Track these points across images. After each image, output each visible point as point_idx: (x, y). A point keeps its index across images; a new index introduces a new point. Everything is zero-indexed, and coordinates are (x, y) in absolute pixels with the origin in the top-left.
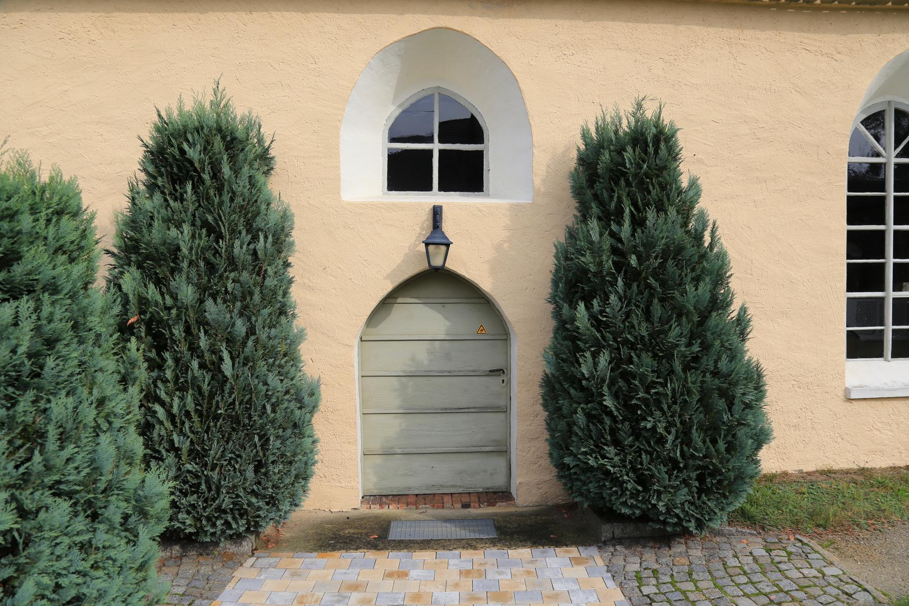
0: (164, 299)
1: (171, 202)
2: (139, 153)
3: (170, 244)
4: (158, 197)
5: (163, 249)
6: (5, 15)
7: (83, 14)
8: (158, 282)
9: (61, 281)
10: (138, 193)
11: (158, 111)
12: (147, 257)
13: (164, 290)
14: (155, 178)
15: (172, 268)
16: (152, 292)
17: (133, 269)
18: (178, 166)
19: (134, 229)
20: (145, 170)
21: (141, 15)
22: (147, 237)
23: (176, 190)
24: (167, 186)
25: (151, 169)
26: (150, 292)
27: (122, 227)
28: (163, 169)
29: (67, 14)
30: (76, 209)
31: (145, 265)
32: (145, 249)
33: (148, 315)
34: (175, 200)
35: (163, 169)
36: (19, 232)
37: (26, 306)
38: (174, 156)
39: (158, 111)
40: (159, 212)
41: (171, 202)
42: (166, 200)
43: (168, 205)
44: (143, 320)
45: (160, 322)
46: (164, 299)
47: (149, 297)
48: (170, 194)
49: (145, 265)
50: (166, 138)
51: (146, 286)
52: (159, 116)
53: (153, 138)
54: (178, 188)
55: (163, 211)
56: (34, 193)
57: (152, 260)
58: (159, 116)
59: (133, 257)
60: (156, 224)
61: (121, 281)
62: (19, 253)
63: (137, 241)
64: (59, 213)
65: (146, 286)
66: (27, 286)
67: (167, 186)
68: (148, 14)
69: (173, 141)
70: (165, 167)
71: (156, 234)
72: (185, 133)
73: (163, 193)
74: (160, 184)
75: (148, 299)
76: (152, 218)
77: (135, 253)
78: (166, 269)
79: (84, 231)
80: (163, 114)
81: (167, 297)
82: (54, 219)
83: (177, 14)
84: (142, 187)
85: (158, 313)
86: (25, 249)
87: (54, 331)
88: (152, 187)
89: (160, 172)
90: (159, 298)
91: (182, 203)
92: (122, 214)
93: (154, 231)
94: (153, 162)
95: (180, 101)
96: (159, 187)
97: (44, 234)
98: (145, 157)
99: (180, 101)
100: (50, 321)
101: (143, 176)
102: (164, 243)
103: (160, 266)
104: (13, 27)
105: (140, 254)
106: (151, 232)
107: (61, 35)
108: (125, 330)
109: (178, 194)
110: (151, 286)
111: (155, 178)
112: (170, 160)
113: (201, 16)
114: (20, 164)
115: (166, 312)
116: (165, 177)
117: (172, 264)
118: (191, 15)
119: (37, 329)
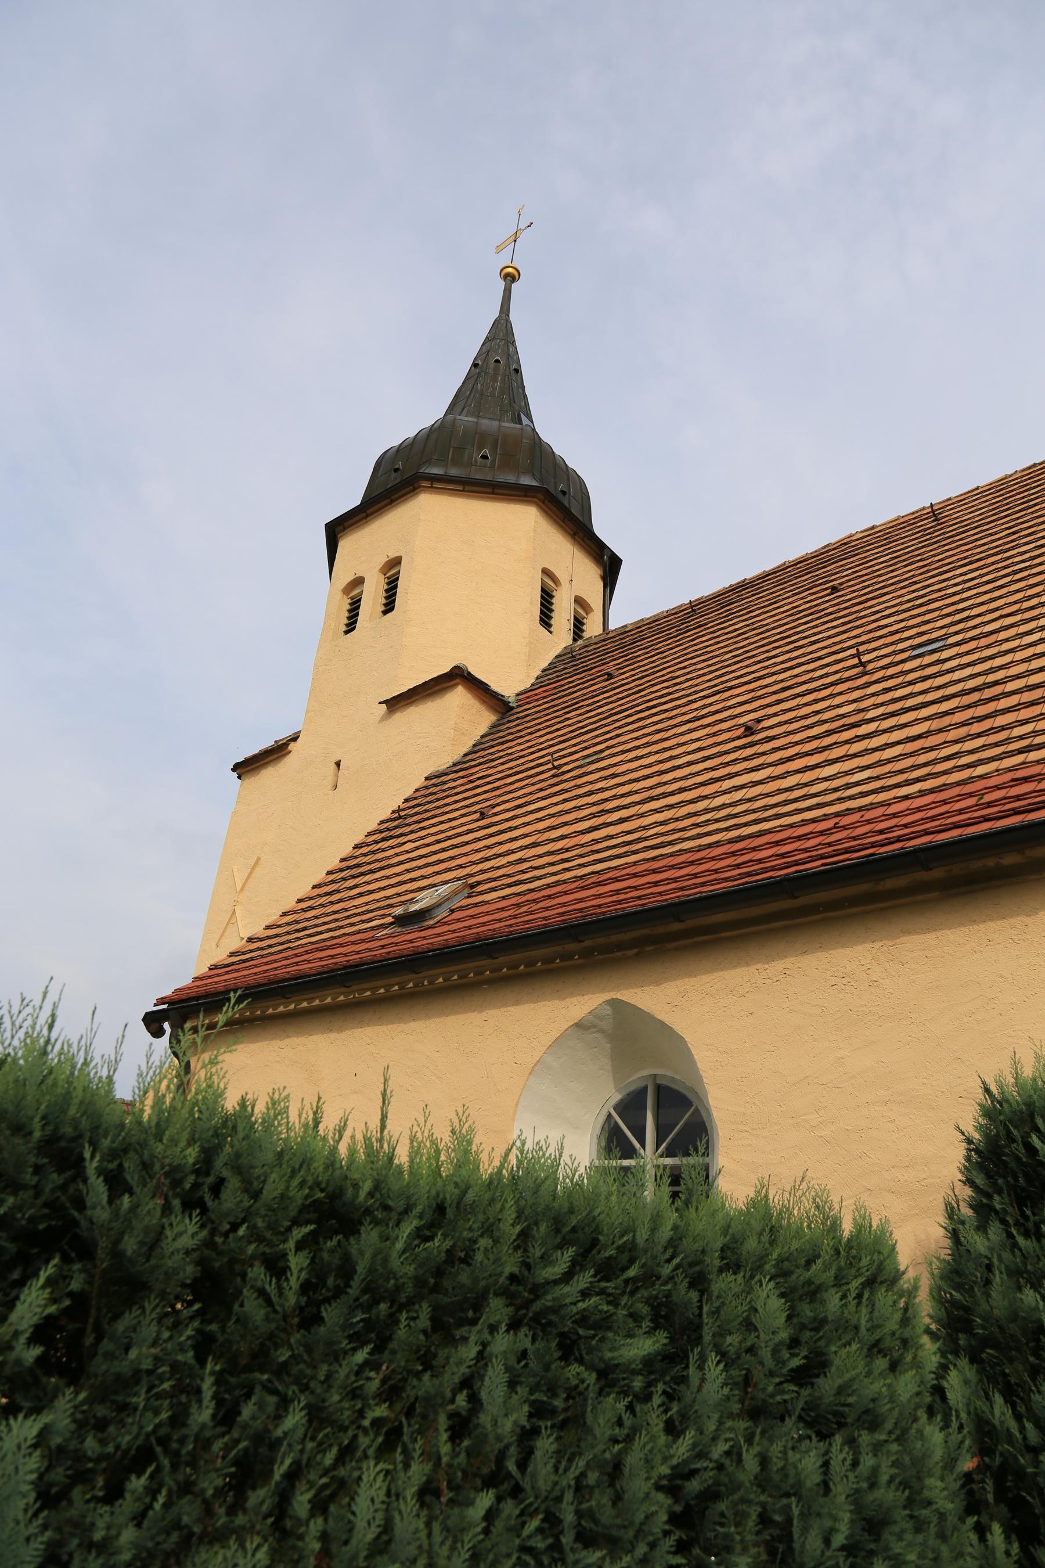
0: (1022, 1429)
1: (1021, 1240)
2: (957, 1154)
3: (1024, 1318)
4: (995, 1230)
5: (1013, 1329)
6: (767, 966)
7: (860, 948)
8: (1010, 1393)
9: (884, 1408)
10: (963, 1223)
11: (984, 1083)
12: (987, 1342)
13: (1021, 1409)
14: (989, 1196)
15: (1032, 1366)
16: (1000, 1411)
17: (963, 1363)
18: (1026, 1175)
19: (958, 1287)
20: (969, 1182)
21: (938, 934)
22: (985, 1306)
23: (1026, 1218)
24: (1010, 1209)
25: (980, 1180)
26: (997, 1412)
27: (940, 1282)
28: (1000, 1181)
29: (840, 950)
30: (893, 1274)
31: (984, 1356)
32: (983, 1327)
33: (998, 1460)
34: (1027, 1235)
35: (1000, 1181)
36: (824, 1321)
37: (841, 1457)
38: (1018, 1159)
39: (984, 1083)
40: (1000, 1257)
41: (1021, 1240)
42: (1010, 1236)
43: (1015, 1245)
44: (988, 1467)
45: (1020, 1474)
46: (1022, 1429)
47: (996, 1422)
48: (1017, 1224)
49: (984, 1356)
50: (1001, 1128)
51: (987, 1397)
52: (987, 1090)
53: (979, 1128)
54: (1028, 1212)
55: (1007, 1255)
56: (838, 1252)
57: (996, 1346)
58: (987, 1090)
59: (963, 1340)
60: (998, 1279)
61: (945, 1384)
62: (824, 1354)
63: (967, 1310)
64: (871, 1283)
65: (987, 1397)
66: (835, 1414)
67: (1010, 1209)
68: (949, 932)
69: (1015, 1132)
70: (1004, 1177)
71: (998, 1300)
72: (1032, 1116)
73: (1003, 1221)
74: (998, 1207)
75: (994, 1427)
76: (989, 1268)
77: (965, 1332)
78: (1021, 1368)
79: (906, 1309)
80: (994, 1089)
81: (1029, 1426)
82: (866, 1295)
83: (991, 924)
84: (966, 1211)
85: (1016, 1459)
86: (833, 1349)
87: (880, 1506)
88: (983, 1210)
89: (994, 1184)
90: (1013, 1425)
91: (1039, 1240)
92: (938, 1258)
93: (993, 1294)
94: (981, 1167)
95: (1015, 1063)
96: (996, 1212)
97: (854, 1321)
98: (968, 1159)
99: (1015, 1063)
100: (873, 1485)
101: (967, 1192)
102: (1014, 1317)
103: (1011, 1360)
104: (775, 979)
105: (974, 1335)
106: (988, 1296)
107: (834, 980)
108: (973, 1506)
109: (1030, 1225)
110: (998, 1399)
111: (989, 1196)
112: (1013, 1165)
113: (1029, 920)
114: (817, 1207)
115: (1029, 1457)
116: (1005, 1195)
117: (1032, 1359)
118: (1013, 921)
119: (856, 1498)
